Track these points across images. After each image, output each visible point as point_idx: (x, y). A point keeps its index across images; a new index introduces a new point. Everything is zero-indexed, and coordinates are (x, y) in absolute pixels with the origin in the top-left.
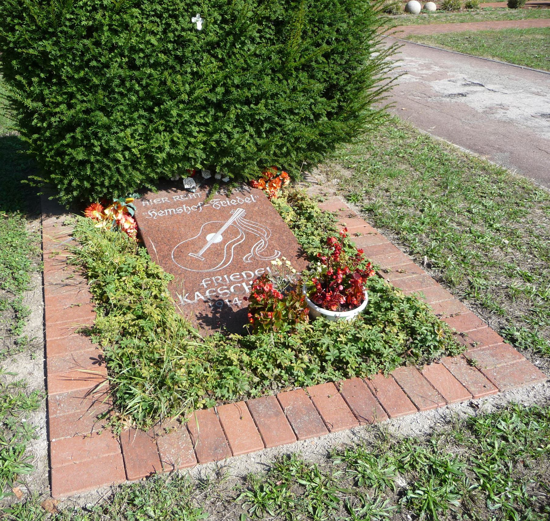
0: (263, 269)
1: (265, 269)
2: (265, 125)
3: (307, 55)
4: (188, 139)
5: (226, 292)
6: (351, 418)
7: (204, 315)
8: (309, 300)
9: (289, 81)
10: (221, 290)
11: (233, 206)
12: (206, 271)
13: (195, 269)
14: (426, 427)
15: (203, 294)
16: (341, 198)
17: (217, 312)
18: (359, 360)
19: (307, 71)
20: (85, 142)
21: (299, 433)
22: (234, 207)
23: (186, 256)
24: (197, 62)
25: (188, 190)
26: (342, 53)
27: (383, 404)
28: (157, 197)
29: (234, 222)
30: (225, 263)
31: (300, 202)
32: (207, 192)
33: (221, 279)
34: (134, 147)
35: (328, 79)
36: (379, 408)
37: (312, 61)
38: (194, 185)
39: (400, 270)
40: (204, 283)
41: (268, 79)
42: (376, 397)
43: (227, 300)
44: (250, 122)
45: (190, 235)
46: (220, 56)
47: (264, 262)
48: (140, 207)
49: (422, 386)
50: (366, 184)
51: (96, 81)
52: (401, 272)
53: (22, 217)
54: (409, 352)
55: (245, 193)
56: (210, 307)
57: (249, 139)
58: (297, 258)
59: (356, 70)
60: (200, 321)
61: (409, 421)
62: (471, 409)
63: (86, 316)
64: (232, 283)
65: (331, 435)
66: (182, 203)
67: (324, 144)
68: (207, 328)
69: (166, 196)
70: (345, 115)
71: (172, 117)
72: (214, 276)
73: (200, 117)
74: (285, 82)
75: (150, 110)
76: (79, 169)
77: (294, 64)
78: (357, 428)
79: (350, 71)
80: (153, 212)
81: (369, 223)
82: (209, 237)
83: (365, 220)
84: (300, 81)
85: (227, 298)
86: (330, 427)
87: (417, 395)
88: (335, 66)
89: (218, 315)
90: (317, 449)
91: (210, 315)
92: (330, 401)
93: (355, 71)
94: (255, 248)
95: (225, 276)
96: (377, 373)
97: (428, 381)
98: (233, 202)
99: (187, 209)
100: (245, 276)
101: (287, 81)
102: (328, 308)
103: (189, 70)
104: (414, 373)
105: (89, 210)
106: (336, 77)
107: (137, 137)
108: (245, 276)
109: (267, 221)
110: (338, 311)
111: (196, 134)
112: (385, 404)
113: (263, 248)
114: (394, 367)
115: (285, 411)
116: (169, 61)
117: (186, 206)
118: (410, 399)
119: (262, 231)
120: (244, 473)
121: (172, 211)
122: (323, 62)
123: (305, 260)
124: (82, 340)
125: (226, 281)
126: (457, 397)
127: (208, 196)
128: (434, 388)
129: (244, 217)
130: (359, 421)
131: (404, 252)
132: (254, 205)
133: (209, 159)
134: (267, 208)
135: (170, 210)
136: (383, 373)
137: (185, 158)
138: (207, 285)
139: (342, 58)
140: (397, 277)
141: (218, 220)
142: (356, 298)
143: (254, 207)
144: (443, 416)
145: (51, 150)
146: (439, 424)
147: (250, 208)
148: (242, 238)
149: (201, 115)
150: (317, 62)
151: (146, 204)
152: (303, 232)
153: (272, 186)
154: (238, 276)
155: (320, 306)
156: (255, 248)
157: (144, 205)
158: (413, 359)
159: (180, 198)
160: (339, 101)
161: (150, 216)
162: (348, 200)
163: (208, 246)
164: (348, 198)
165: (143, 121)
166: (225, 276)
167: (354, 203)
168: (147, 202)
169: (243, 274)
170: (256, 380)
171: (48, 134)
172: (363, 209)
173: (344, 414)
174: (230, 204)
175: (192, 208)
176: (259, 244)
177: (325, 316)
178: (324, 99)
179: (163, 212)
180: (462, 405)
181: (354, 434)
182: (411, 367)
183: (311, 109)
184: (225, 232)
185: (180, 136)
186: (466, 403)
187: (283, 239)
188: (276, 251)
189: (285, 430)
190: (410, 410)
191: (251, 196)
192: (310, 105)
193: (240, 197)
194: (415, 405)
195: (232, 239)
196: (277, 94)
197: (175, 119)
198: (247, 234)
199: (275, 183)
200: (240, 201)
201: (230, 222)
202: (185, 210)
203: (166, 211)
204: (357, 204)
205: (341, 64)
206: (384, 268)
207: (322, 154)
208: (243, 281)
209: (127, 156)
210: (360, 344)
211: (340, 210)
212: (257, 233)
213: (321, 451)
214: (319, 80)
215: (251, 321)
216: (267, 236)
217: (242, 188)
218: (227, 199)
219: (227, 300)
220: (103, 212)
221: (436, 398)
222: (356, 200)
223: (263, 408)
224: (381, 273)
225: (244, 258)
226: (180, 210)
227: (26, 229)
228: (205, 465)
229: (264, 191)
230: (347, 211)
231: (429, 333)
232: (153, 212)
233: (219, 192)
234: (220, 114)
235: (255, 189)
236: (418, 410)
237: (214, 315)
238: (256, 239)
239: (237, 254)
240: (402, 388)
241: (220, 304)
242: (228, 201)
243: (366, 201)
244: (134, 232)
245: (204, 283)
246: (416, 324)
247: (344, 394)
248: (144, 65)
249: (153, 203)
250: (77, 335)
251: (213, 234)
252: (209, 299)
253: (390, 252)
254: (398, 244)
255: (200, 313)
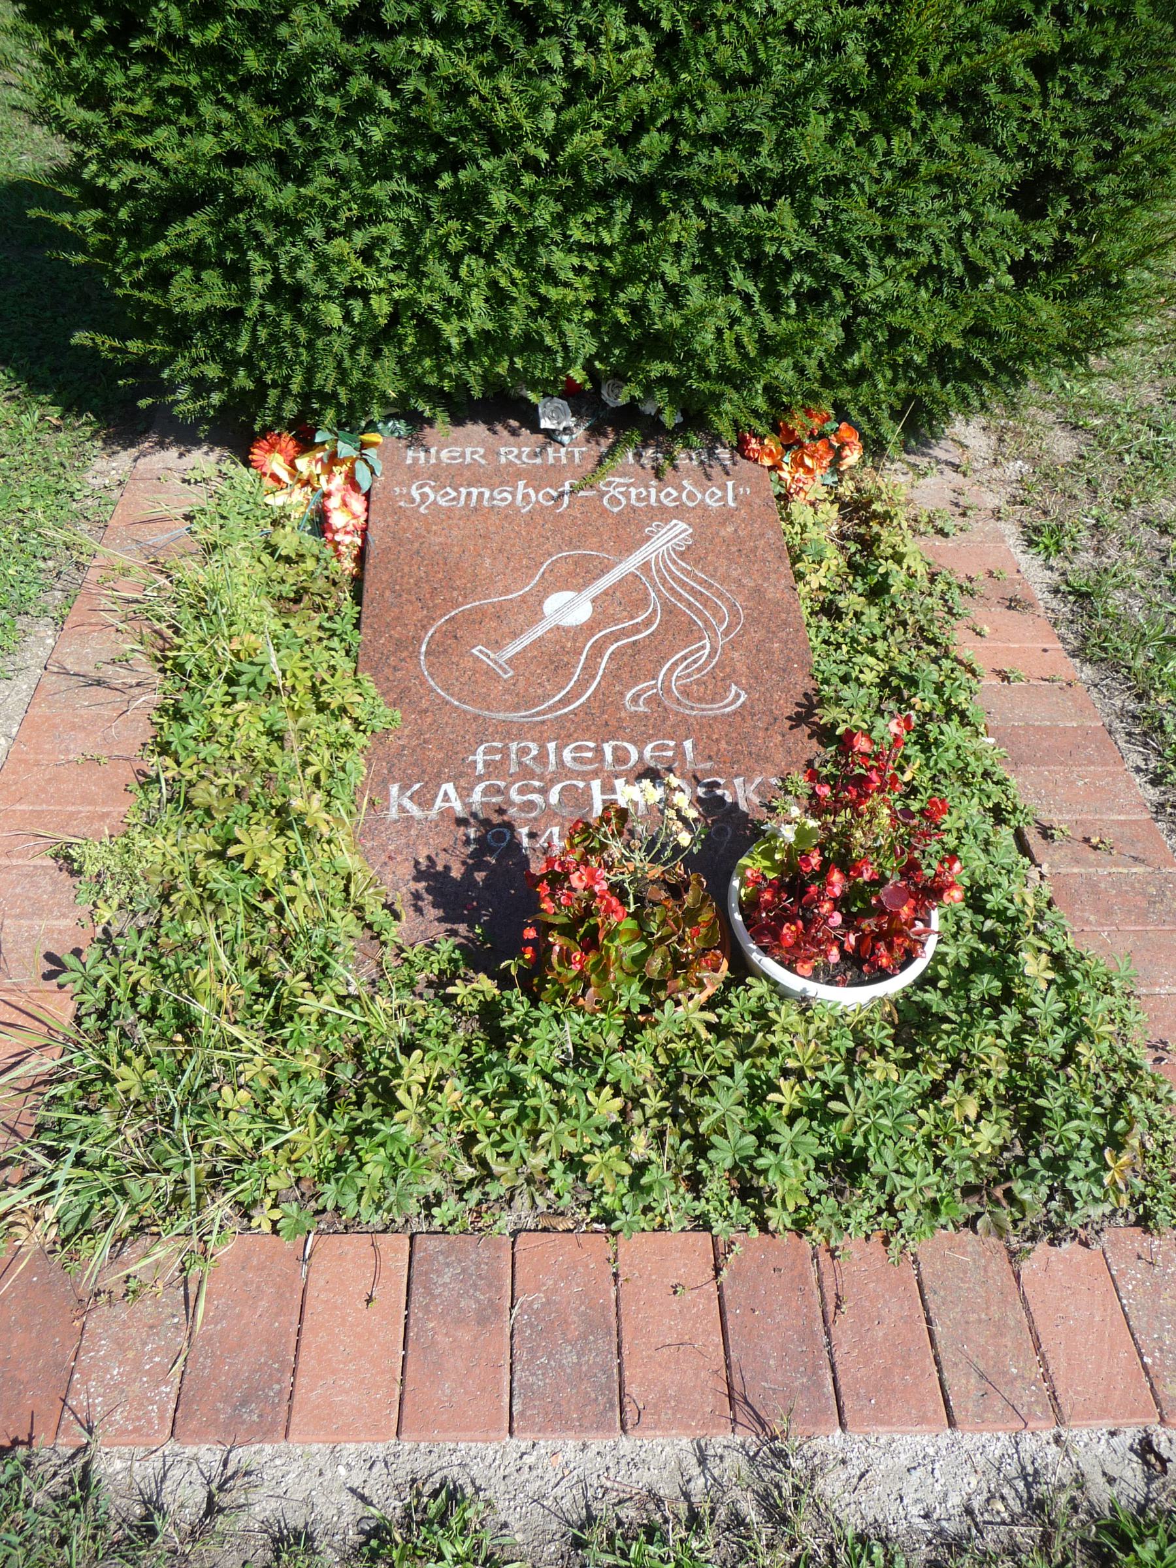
0: (672, 743)
1: (679, 746)
2: (796, 277)
3: (969, 56)
4: (543, 290)
5: (531, 802)
6: (713, 1400)
7: (440, 868)
8: (738, 917)
9: (895, 141)
10: (521, 792)
11: (663, 508)
12: (502, 716)
13: (473, 702)
14: (955, 1500)
15: (464, 793)
16: (1010, 531)
17: (479, 865)
18: (819, 1182)
19: (965, 114)
20: (229, 256)
21: (522, 1413)
22: (664, 514)
23: (462, 656)
24: (590, 38)
25: (550, 434)
26: (1103, 61)
27: (839, 1368)
28: (456, 442)
29: (646, 567)
30: (564, 702)
31: (876, 528)
32: (604, 449)
33: (534, 752)
34: (380, 291)
35: (1033, 149)
36: (820, 1385)
37: (987, 80)
38: (570, 421)
39: (1094, 840)
40: (479, 758)
41: (818, 127)
42: (828, 1333)
43: (524, 831)
44: (746, 262)
45: (500, 586)
46: (665, 24)
47: (685, 719)
48: (394, 465)
49: (1000, 1328)
50: (1105, 495)
51: (252, 61)
52: (1095, 848)
53: (94, 435)
54: (998, 1192)
55: (716, 471)
56: (467, 842)
57: (738, 314)
58: (788, 723)
59: (1144, 128)
60: (422, 885)
61: (904, 1460)
62: (1136, 1464)
63: (104, 803)
64: (563, 771)
65: (626, 1445)
66: (518, 475)
67: (986, 362)
68: (432, 913)
69: (482, 443)
70: (1075, 278)
71: (492, 214)
72: (519, 737)
73: (586, 224)
74: (879, 142)
75: (425, 178)
76: (223, 334)
77: (919, 83)
78: (720, 1440)
79: (1121, 130)
80: (427, 489)
81: (1063, 640)
82: (554, 603)
83: (1055, 625)
84: (931, 149)
85: (527, 822)
86: (631, 1417)
87: (970, 1363)
88: (1069, 107)
89: (479, 876)
90: (559, 1491)
91: (456, 873)
92: (675, 1307)
93: (1137, 134)
94: (676, 664)
95: (551, 746)
96: (868, 1237)
97: (1029, 1313)
98: (668, 496)
99: (526, 496)
100: (609, 757)
101: (889, 140)
102: (790, 967)
103: (557, 61)
104: (993, 1267)
105: (260, 448)
106: (1063, 144)
107: (386, 262)
108: (609, 757)
109: (744, 581)
110: (815, 978)
111: (571, 275)
112: (846, 1371)
113: (699, 670)
114: (932, 1228)
115: (515, 1311)
116: (488, 22)
117: (526, 486)
118: (940, 1371)
119: (716, 610)
120: (296, 1520)
121: (481, 494)
122: (1026, 85)
123: (810, 737)
124: (54, 882)
125: (545, 764)
126: (1104, 1413)
127: (600, 463)
128: (1038, 1348)
129: (681, 555)
130: (734, 1420)
131: (1138, 770)
132: (726, 516)
133: (608, 358)
134: (762, 535)
135: (475, 491)
136: (886, 1242)
137: (531, 344)
138: (487, 764)
139: (1097, 81)
140: (1077, 861)
141: (601, 547)
142: (890, 948)
143: (723, 524)
144: (1030, 1469)
145: (137, 264)
146: (1000, 1506)
147: (709, 526)
148: (648, 623)
149: (590, 218)
150: (1006, 85)
151: (416, 460)
152: (844, 635)
153: (802, 464)
154: (589, 755)
155: (765, 950)
156: (676, 664)
157: (409, 461)
158: (1006, 1214)
159: (518, 457)
160: (1064, 227)
161: (413, 501)
162: (1031, 543)
163: (539, 634)
164: (1031, 537)
165: (407, 212)
166: (551, 746)
167: (1042, 557)
168: (422, 455)
169: (608, 748)
170: (467, 1172)
171: (123, 214)
172: (1063, 587)
173: (697, 1376)
174: (658, 500)
175: (538, 497)
176: (692, 653)
177: (776, 988)
178: (1011, 215)
179: (454, 494)
180: (1115, 1441)
181: (702, 1461)
182: (993, 1240)
183: (958, 245)
184: (606, 593)
185: (517, 274)
186: (1130, 1437)
187: (770, 652)
188: (734, 688)
189: (483, 1390)
190: (923, 1420)
191: (730, 484)
192: (959, 231)
193: (696, 484)
194: (946, 1402)
195: (617, 621)
196: (844, 181)
197: (501, 221)
198: (670, 611)
199: (812, 457)
200: (691, 497)
201: (630, 564)
202: (519, 497)
203: (463, 491)
204: (1052, 562)
205: (1089, 103)
206: (1045, 818)
207: (980, 393)
208: (596, 774)
209: (356, 314)
210: (837, 1131)
211: (991, 574)
212: (699, 613)
213: (566, 1504)
214: (999, 151)
215: (527, 956)
216: (726, 633)
217: (711, 453)
218: (654, 483)
219: (524, 831)
220: (292, 464)
221: (1029, 1395)
222: (1052, 549)
223: (454, 1277)
224: (1033, 837)
225: (629, 695)
226: (503, 497)
227: (91, 473)
228: (190, 1451)
229: (774, 476)
230: (1012, 584)
231: (1086, 1143)
232: (427, 489)
233: (638, 455)
234: (645, 225)
235: (750, 463)
236: (952, 1424)
237: (469, 871)
238: (690, 633)
239: (613, 675)
240: (929, 1321)
241: (500, 837)
242: (653, 491)
243: (1087, 557)
244: (349, 542)
245: (479, 758)
246: (1051, 1102)
247: (727, 1293)
248: (410, 28)
249: (438, 458)
250: (51, 862)
251: (568, 595)
252: (474, 815)
253: (1092, 763)
254: (1129, 734)
255: (429, 858)
